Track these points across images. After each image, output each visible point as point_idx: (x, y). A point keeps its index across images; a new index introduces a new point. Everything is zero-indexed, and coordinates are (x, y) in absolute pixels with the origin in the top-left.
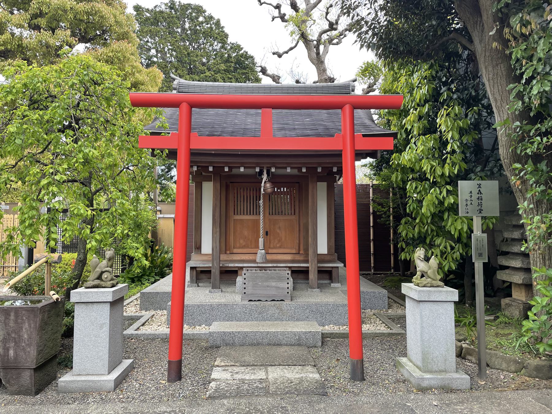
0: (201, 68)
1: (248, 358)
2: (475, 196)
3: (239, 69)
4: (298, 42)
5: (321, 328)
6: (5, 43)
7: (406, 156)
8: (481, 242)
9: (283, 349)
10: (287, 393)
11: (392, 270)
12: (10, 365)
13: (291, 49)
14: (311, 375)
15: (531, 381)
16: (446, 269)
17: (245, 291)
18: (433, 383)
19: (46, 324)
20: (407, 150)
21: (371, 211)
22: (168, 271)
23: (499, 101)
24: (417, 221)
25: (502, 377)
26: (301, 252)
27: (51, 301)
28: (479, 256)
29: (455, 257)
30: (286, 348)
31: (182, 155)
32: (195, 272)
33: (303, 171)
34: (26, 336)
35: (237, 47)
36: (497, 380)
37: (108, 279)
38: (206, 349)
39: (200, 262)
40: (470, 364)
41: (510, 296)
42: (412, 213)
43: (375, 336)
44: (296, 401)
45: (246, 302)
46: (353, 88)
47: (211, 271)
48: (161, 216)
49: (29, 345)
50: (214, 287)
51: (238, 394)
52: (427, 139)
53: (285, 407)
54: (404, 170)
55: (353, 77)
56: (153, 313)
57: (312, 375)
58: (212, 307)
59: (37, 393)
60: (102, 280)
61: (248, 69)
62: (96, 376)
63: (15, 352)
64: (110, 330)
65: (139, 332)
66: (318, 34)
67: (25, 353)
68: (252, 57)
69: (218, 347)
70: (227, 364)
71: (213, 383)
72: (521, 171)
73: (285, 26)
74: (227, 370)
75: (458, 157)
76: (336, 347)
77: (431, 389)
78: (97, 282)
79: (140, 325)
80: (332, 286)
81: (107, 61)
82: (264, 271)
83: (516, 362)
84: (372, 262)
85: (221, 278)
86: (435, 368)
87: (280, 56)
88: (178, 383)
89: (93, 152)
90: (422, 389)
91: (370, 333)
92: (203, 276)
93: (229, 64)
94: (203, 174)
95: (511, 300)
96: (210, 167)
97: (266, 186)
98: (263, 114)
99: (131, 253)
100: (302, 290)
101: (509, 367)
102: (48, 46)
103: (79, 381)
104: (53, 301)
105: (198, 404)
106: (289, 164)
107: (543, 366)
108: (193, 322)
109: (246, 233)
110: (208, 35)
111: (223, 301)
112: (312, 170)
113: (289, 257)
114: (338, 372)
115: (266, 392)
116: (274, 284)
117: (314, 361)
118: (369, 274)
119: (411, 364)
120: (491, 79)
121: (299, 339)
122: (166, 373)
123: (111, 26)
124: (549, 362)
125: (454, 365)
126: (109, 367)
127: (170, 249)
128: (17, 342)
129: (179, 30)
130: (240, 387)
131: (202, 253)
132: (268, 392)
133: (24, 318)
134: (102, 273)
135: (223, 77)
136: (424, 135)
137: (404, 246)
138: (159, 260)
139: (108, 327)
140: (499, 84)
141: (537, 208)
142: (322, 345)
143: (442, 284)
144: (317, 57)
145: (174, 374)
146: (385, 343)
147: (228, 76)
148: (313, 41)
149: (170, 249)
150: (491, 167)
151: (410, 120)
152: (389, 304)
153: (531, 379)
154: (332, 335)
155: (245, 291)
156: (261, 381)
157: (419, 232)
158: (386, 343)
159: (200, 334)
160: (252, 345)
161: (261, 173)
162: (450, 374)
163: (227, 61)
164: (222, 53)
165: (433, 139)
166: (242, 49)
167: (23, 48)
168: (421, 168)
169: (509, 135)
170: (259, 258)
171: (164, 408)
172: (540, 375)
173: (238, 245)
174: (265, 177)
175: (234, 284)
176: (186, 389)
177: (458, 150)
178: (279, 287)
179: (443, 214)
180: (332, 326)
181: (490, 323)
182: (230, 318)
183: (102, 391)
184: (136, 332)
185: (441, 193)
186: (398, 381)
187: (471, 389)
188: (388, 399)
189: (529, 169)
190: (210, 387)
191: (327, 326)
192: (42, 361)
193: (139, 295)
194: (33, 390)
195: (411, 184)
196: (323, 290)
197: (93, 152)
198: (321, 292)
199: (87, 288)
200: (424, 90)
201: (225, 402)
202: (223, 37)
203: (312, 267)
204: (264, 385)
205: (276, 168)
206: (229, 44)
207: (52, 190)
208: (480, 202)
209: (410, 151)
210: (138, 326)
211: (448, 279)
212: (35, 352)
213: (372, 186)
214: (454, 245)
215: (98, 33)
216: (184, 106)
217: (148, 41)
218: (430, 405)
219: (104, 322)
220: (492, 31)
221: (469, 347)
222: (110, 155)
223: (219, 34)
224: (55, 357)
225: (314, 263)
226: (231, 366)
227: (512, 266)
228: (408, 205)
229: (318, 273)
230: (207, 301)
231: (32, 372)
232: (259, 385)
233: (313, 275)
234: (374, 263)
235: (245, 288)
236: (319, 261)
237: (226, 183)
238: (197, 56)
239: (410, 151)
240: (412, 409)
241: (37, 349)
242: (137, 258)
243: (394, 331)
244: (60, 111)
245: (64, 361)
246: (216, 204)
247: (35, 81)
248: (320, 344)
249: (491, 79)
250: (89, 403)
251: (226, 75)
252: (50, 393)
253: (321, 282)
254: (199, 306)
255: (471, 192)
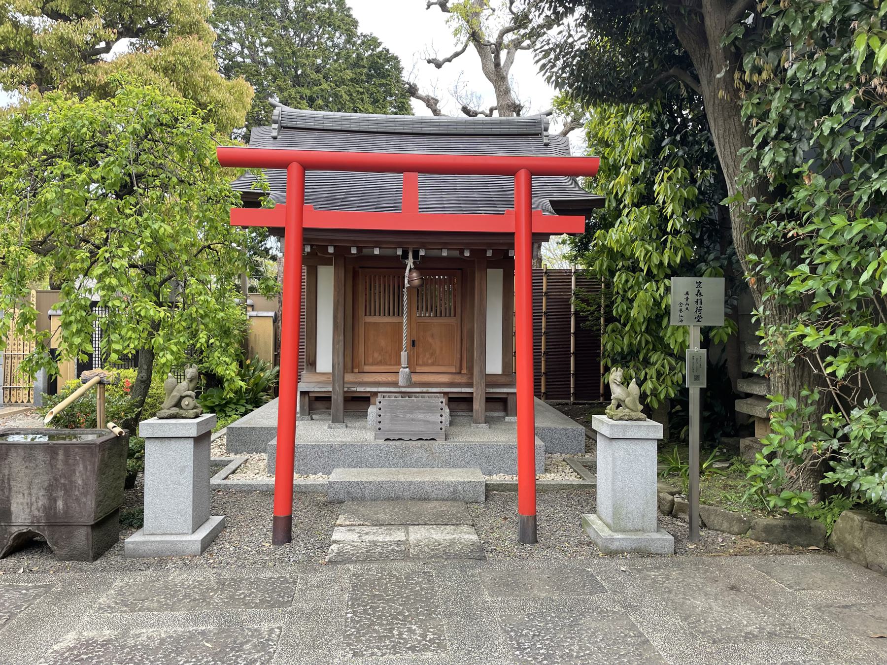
0: (314, 76)
1: (381, 516)
2: (693, 298)
3: (374, 77)
4: (466, 46)
5: (487, 478)
6: (5, 40)
7: (613, 235)
8: (699, 360)
9: (431, 505)
10: (432, 557)
11: (601, 398)
12: (58, 521)
13: (457, 55)
14: (466, 537)
15: (758, 545)
16: (662, 396)
17: (380, 426)
18: (625, 544)
19: (106, 466)
20: (616, 226)
21: (572, 310)
22: (264, 397)
23: (731, 168)
24: (627, 328)
25: (720, 540)
26: (464, 371)
27: (112, 436)
28: (695, 379)
29: (675, 381)
30: (436, 503)
31: (293, 234)
32: (307, 399)
33: (465, 255)
34: (80, 482)
35: (371, 42)
36: (712, 544)
37: (188, 408)
38: (325, 504)
39: (314, 385)
40: (681, 524)
41: (753, 434)
42: (620, 316)
43: (559, 488)
44: (444, 566)
45: (382, 442)
46: (546, 125)
47: (331, 397)
48: (254, 313)
49: (85, 494)
50: (335, 421)
51: (368, 557)
52: (642, 212)
53: (428, 572)
54: (612, 255)
55: (548, 107)
56: (246, 457)
57: (468, 536)
58: (332, 448)
59: (95, 558)
60: (181, 408)
61: (389, 78)
62: (175, 536)
63: (66, 504)
64: (194, 475)
65: (228, 482)
66: (498, 32)
67: (79, 504)
68: (396, 58)
69: (340, 502)
70: (354, 523)
71: (334, 545)
72: (756, 264)
73: (447, 21)
74: (354, 530)
75: (684, 239)
76: (506, 502)
77: (622, 552)
78: (175, 410)
79: (229, 472)
80: (506, 420)
81: (166, 69)
82: (407, 398)
83: (740, 520)
84: (572, 386)
85: (345, 408)
86: (629, 526)
87: (439, 65)
88: (287, 545)
89: (165, 229)
90: (611, 553)
91: (553, 485)
92: (318, 404)
93: (359, 70)
94: (319, 254)
95: (752, 441)
96: (329, 247)
97: (411, 277)
98: (405, 181)
99: (220, 371)
100: (463, 425)
101: (731, 527)
102: (70, 43)
103: (153, 542)
104: (114, 436)
105: (315, 569)
106: (445, 245)
107: (775, 526)
108: (306, 469)
109: (383, 343)
110: (325, 23)
111: (348, 439)
112: (479, 253)
113: (445, 379)
114: (504, 533)
115: (405, 556)
116: (421, 416)
117: (473, 520)
118: (567, 404)
119: (600, 522)
120: (721, 136)
121: (454, 492)
122: (270, 534)
123: (171, 12)
124: (783, 521)
125: (655, 522)
126: (193, 524)
127: (268, 364)
128: (68, 491)
129: (278, 11)
130: (370, 550)
131: (317, 371)
132: (408, 556)
133: (78, 458)
134: (182, 398)
135: (350, 91)
136: (638, 206)
137: (609, 364)
138: (252, 380)
139: (192, 470)
140: (732, 144)
141: (780, 314)
142: (486, 500)
143: (643, 416)
144: (496, 71)
145: (281, 535)
146: (572, 498)
147: (357, 89)
148: (490, 45)
149: (268, 364)
150: (729, 255)
151: (619, 182)
152: (586, 446)
153: (758, 543)
154: (501, 487)
155: (380, 426)
156: (399, 543)
157: (630, 345)
158: (575, 498)
159: (315, 485)
160: (389, 499)
161: (405, 256)
162: (648, 534)
163: (356, 65)
164: (348, 53)
165: (649, 212)
166: (380, 44)
167: (34, 47)
168: (633, 254)
169: (742, 215)
170: (402, 381)
171: (269, 574)
172: (771, 538)
173: (371, 360)
174: (410, 263)
175: (364, 416)
176: (297, 552)
177: (683, 230)
178: (428, 421)
179: (662, 320)
180: (502, 474)
181: (719, 472)
182: (358, 463)
183: (185, 556)
184: (225, 482)
185: (658, 289)
186: (581, 543)
187: (675, 553)
188: (564, 564)
189: (768, 262)
190: (330, 551)
191: (495, 475)
192: (102, 515)
193: (225, 430)
194: (91, 554)
195: (620, 275)
196: (493, 426)
197: (165, 229)
198: (490, 428)
199: (160, 418)
200: (639, 141)
201: (351, 567)
202: (349, 25)
203: (478, 393)
204: (403, 548)
205: (426, 249)
206: (359, 37)
207: (110, 282)
208: (699, 306)
209: (620, 228)
210: (226, 475)
211: (673, 411)
212: (93, 503)
213: (574, 273)
214: (673, 363)
215: (151, 22)
216: (295, 167)
217: (227, 30)
218: (616, 570)
219: (185, 464)
220: (719, 72)
221: (682, 501)
222: (187, 231)
223: (343, 20)
224: (117, 511)
225: (480, 388)
226: (359, 525)
227: (755, 393)
228: (615, 305)
229: (486, 401)
230: (326, 440)
231: (90, 530)
232: (396, 548)
233: (478, 404)
234: (575, 388)
235: (380, 422)
236: (488, 385)
237: (354, 268)
238: (308, 56)
239: (620, 228)
240: (592, 574)
241: (96, 499)
242: (229, 378)
243: (586, 483)
244: (116, 170)
245: (127, 518)
246: (338, 301)
247: (78, 124)
248: (483, 499)
249: (721, 136)
250: (168, 570)
251: (355, 87)
252: (113, 558)
253: (492, 414)
254: (313, 447)
255: (687, 293)
